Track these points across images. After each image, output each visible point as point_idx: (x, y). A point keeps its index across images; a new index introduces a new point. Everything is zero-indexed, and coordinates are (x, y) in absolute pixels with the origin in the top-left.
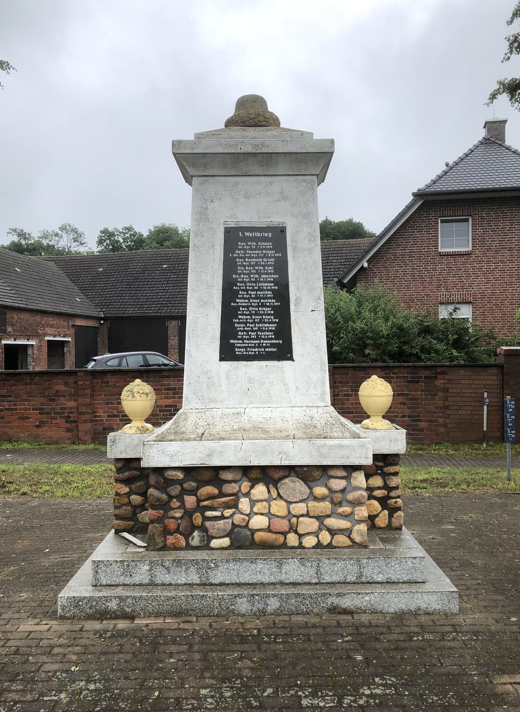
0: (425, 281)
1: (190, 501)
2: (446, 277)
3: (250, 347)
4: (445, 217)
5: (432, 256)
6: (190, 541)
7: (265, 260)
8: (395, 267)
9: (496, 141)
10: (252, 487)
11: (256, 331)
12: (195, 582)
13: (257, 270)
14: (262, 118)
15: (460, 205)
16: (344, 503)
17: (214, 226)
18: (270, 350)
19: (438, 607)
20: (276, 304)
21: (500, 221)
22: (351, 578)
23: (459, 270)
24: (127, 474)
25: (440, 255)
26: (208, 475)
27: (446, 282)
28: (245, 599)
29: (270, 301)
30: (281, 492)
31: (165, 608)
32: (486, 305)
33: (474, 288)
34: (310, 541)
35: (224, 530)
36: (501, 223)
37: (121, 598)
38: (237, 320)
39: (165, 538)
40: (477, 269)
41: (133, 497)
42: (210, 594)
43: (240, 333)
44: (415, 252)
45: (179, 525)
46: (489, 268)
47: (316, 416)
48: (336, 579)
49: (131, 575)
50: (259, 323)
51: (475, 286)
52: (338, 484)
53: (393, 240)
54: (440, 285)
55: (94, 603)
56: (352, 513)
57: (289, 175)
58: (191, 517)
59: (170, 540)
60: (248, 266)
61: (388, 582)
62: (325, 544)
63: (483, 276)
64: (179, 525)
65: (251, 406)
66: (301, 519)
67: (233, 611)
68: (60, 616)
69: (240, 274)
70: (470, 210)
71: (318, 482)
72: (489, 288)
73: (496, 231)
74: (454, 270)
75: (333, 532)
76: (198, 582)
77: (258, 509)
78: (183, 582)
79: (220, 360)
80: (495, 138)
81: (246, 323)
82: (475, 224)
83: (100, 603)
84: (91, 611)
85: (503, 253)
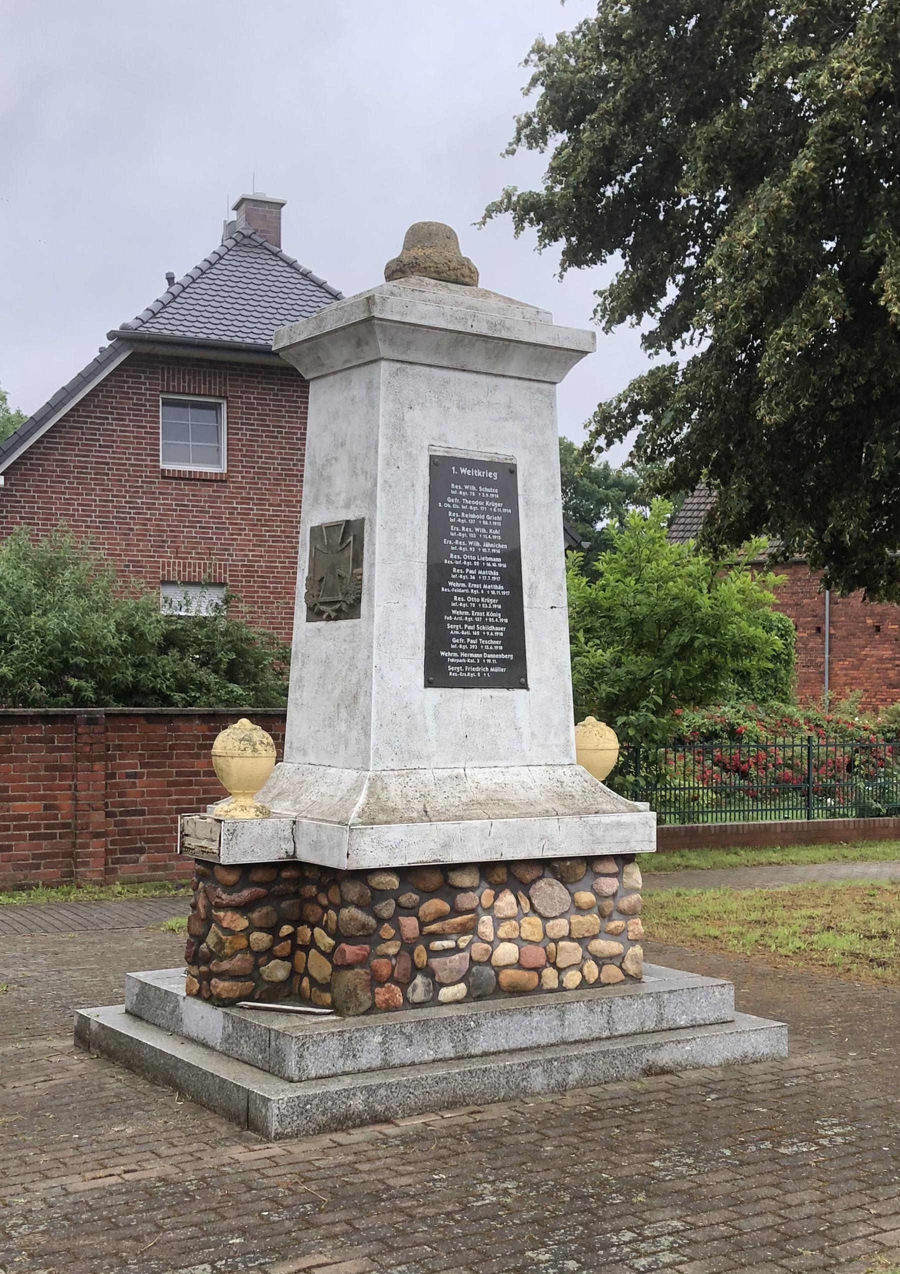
0: (132, 529)
1: (410, 925)
2: (176, 526)
3: (469, 665)
4: (174, 393)
5: (146, 477)
6: (410, 995)
7: (489, 517)
8: (64, 493)
9: (266, 244)
10: (496, 897)
11: (472, 640)
12: (448, 1055)
13: (478, 534)
14: (466, 271)
15: (205, 372)
16: (615, 915)
17: (414, 452)
18: (496, 670)
19: (766, 1050)
20: (504, 593)
21: (284, 417)
22: (650, 1025)
23: (202, 512)
24: (246, 893)
25: (164, 477)
26: (435, 880)
27: (175, 537)
28: (541, 1068)
29: (496, 587)
30: (535, 902)
31: (434, 1097)
32: (255, 592)
33: (231, 555)
34: (572, 978)
35: (459, 971)
36: (286, 422)
37: (370, 1090)
38: (450, 618)
39: (373, 992)
40: (239, 514)
41: (255, 936)
42: (493, 1066)
43: (454, 640)
44: (108, 464)
45: (393, 968)
46: (263, 515)
47: (564, 778)
48: (631, 1028)
49: (354, 1056)
50: (481, 624)
51: (235, 550)
52: (609, 885)
53: (60, 432)
54: (164, 541)
55: (330, 1103)
56: (625, 930)
57: (519, 378)
58: (411, 952)
59: (382, 994)
60: (466, 525)
61: (693, 1026)
62: (592, 980)
63: (250, 530)
64: (393, 968)
65: (469, 764)
66: (561, 944)
67: (524, 1091)
68: (277, 1134)
69: (453, 539)
70: (225, 385)
71: (580, 885)
72: (261, 556)
73: (276, 437)
74: (192, 511)
75: (600, 961)
76: (452, 1055)
77: (505, 932)
78: (431, 1058)
79: (425, 687)
80: (261, 237)
81: (463, 623)
82: (235, 418)
83: (338, 1102)
84: (324, 1118)
85: (289, 486)
